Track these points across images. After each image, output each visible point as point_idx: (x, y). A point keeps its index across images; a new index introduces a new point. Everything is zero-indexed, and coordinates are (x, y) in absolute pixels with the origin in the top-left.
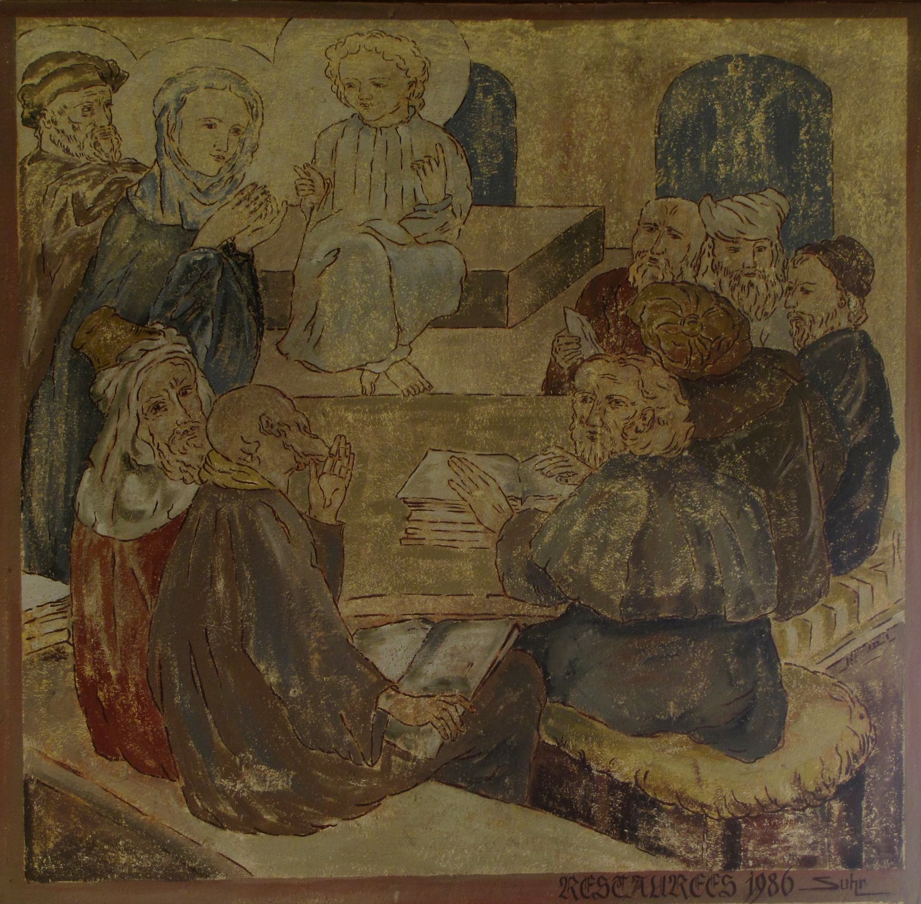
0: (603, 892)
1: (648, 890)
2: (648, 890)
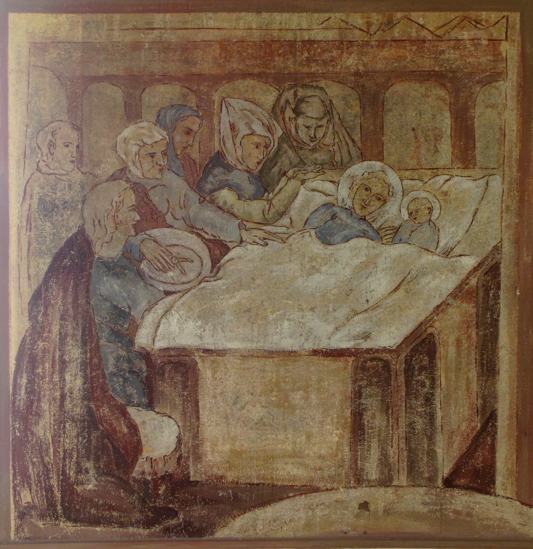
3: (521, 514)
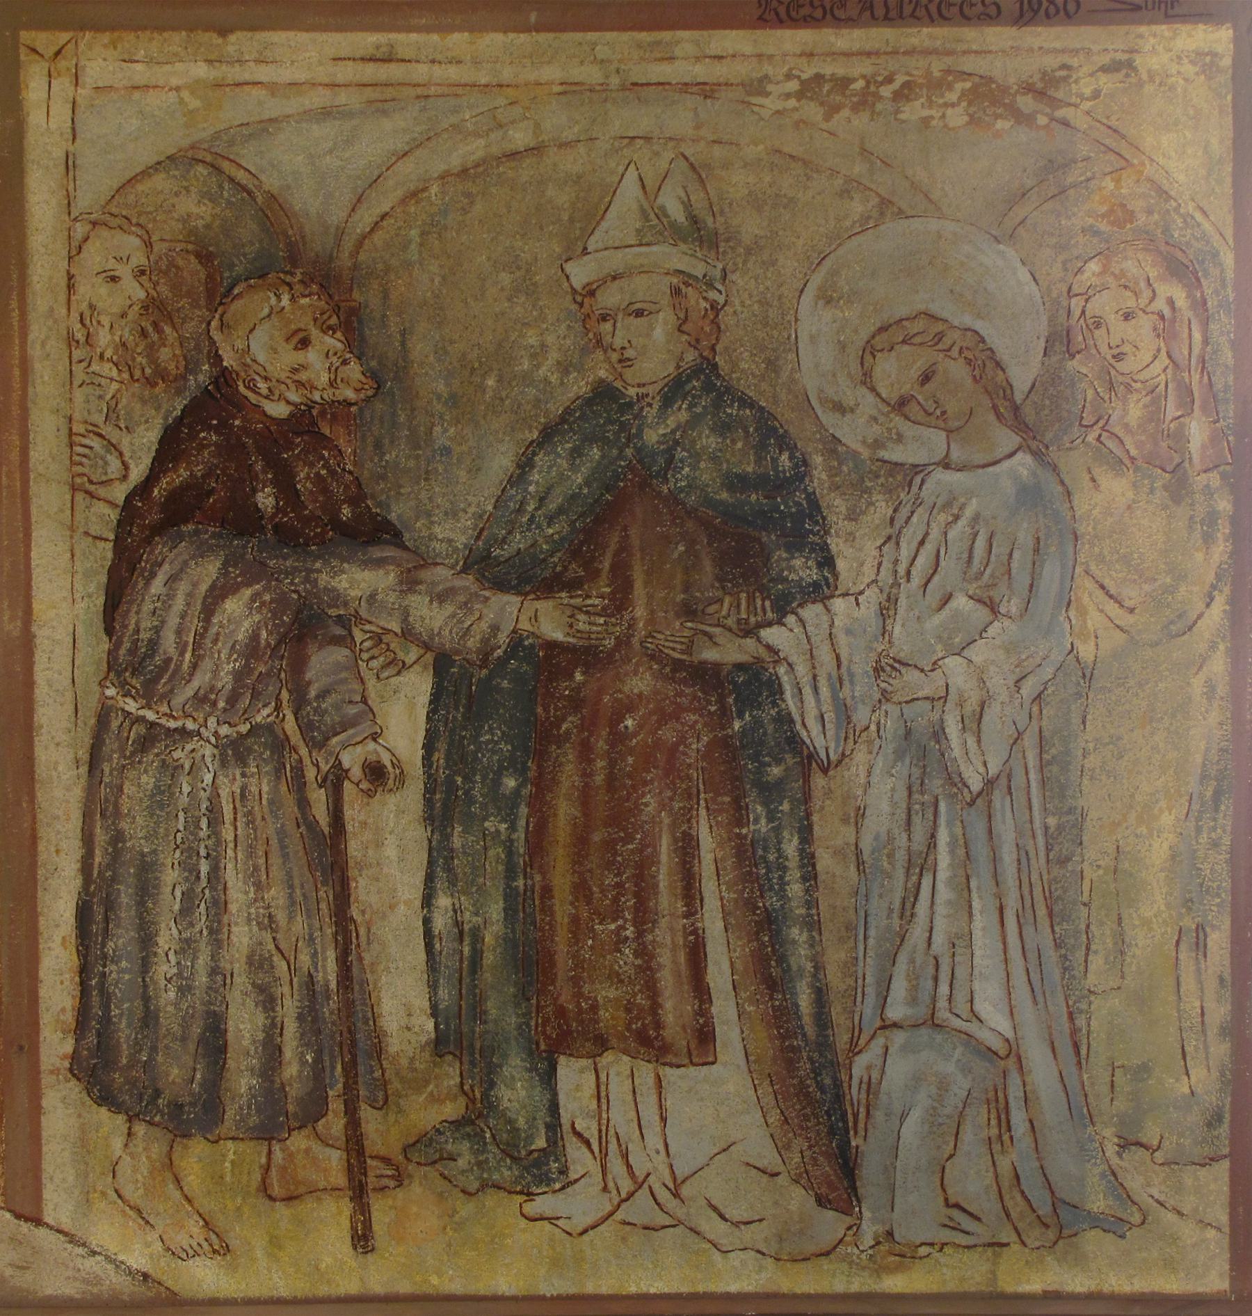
0: (818, 13)
1: (880, 12)
2: (880, 12)
3: (15, 1241)
